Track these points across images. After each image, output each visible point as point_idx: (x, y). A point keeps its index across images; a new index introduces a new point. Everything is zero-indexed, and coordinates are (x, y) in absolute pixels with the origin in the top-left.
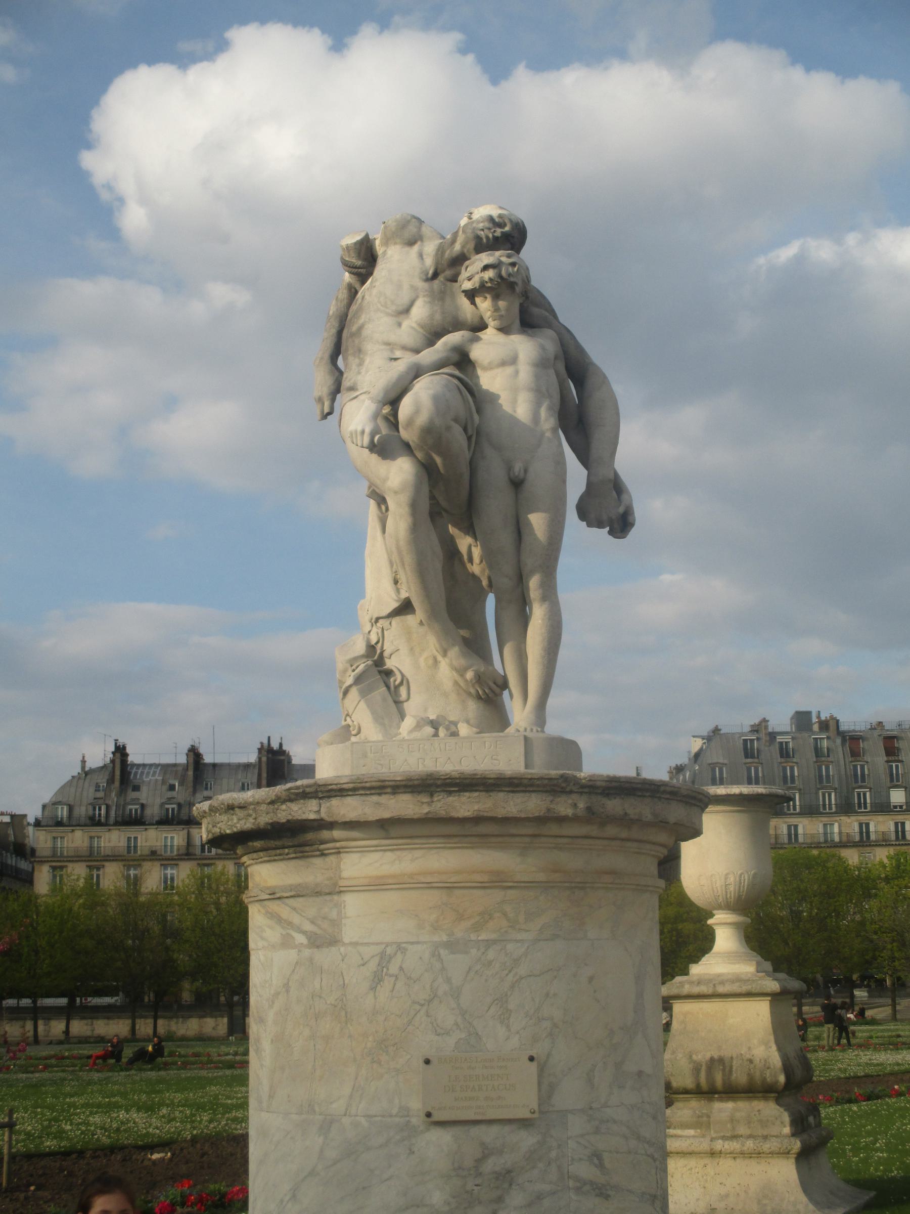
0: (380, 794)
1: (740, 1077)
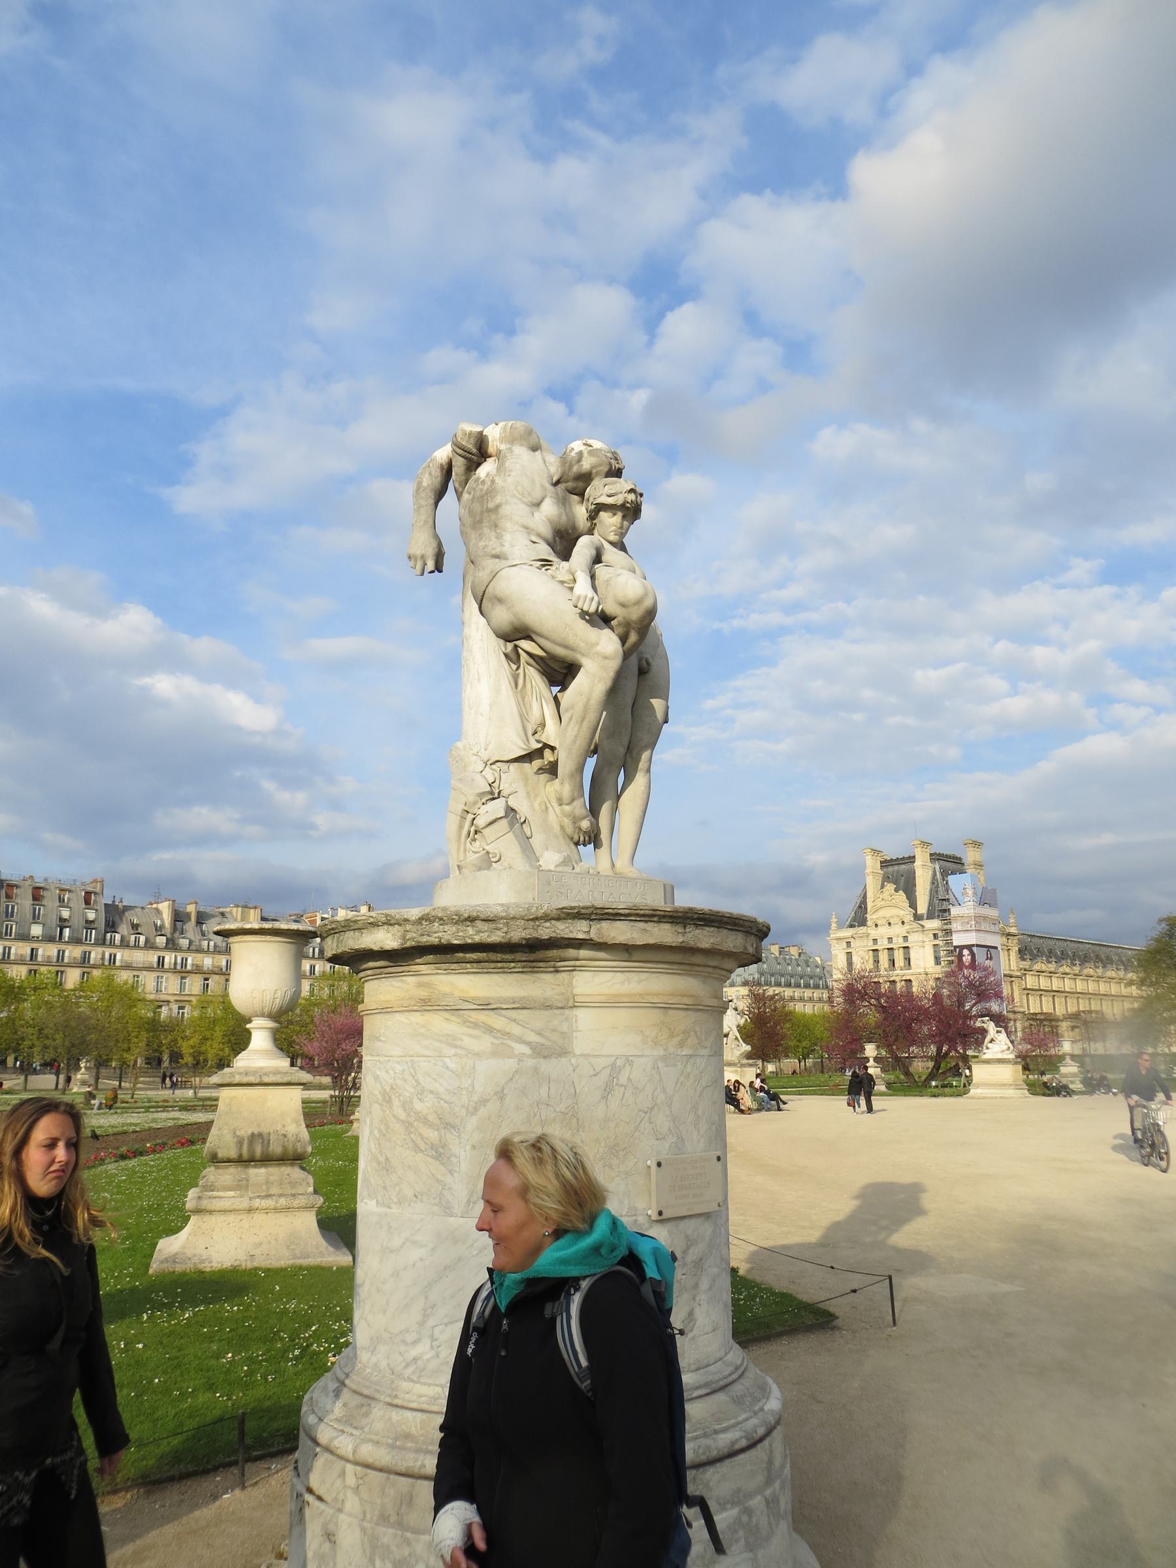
0: (646, 922)
1: (276, 1149)
